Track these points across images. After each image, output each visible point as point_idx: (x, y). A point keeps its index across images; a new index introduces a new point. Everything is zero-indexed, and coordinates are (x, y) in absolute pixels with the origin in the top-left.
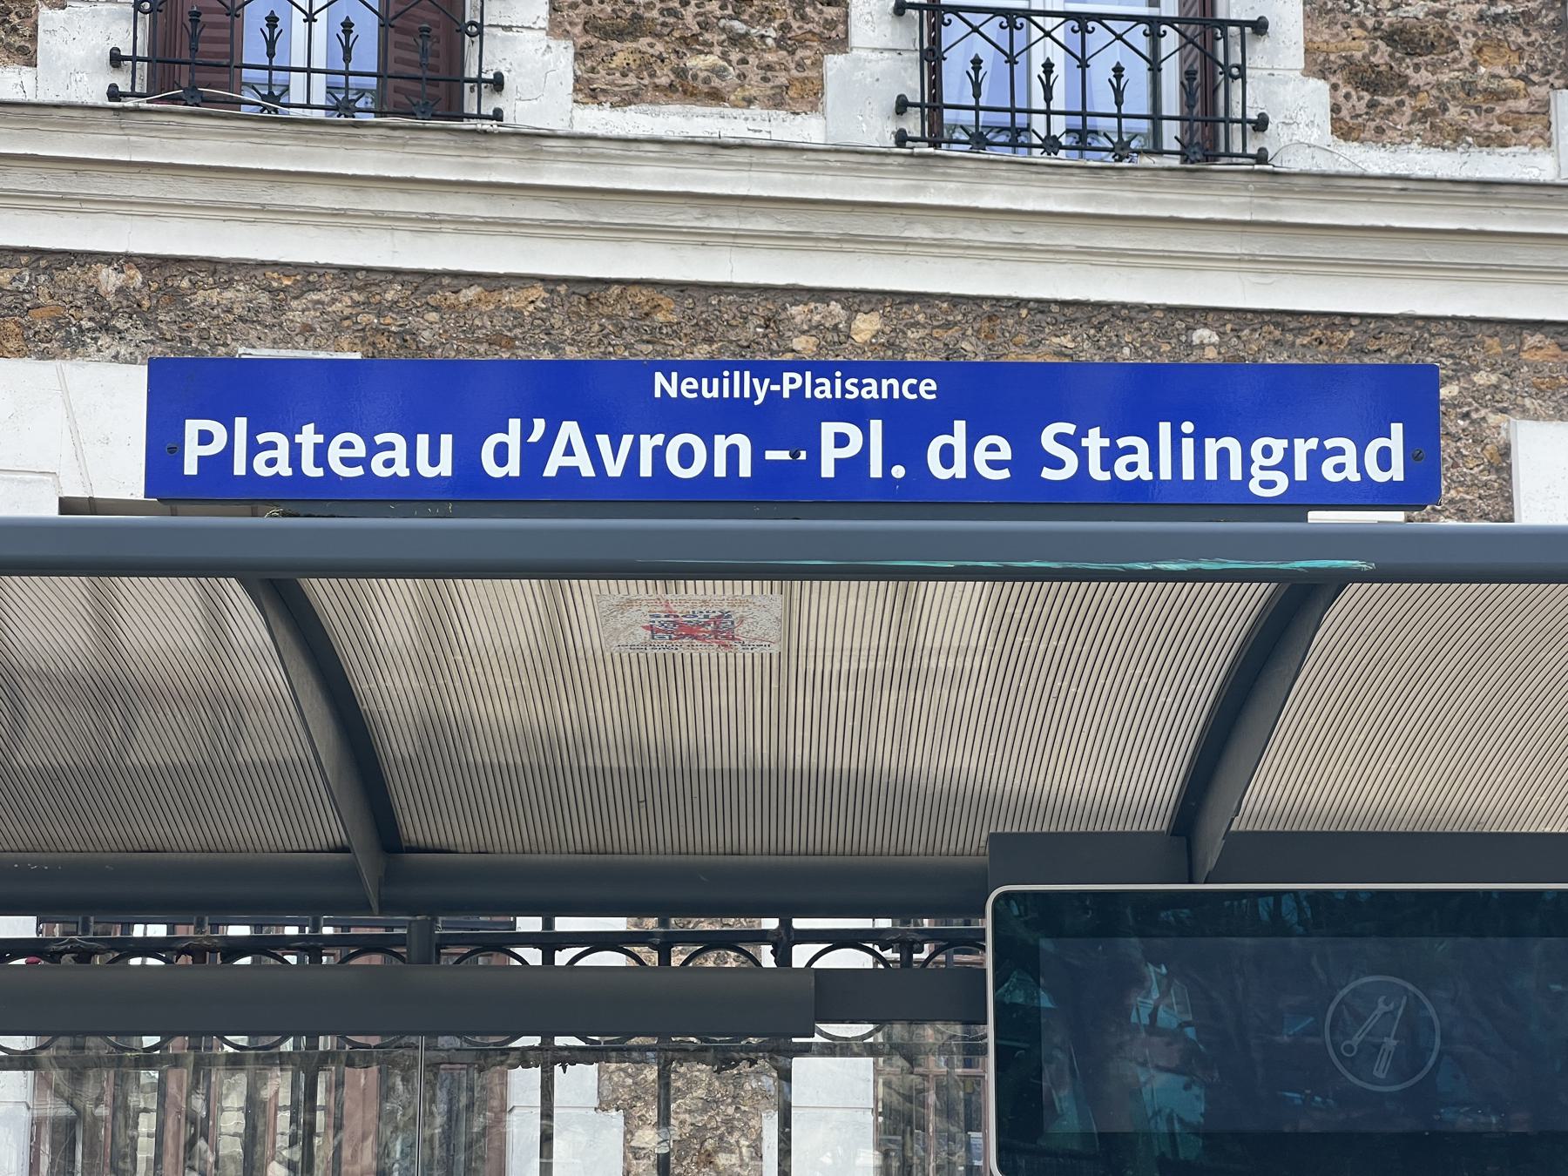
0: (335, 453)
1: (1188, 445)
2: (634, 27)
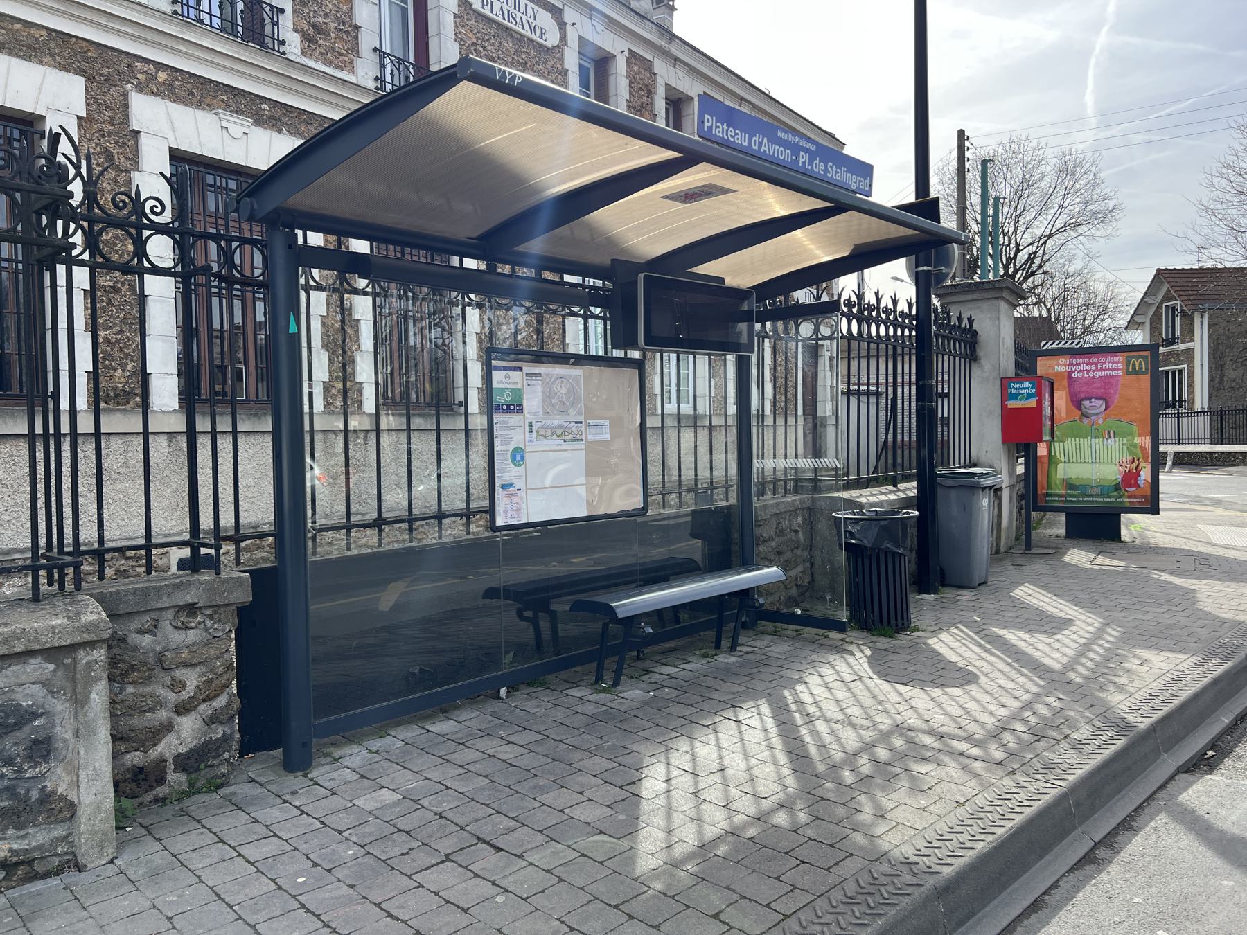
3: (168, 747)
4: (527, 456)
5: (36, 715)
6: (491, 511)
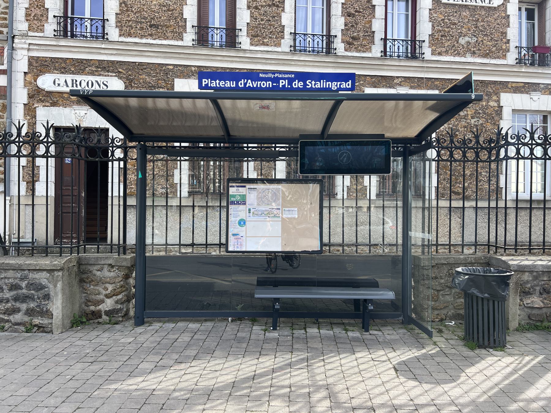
0: (221, 84)
1: (325, 83)
2: (257, 36)
3: (103, 307)
4: (247, 223)
6: (227, 245)
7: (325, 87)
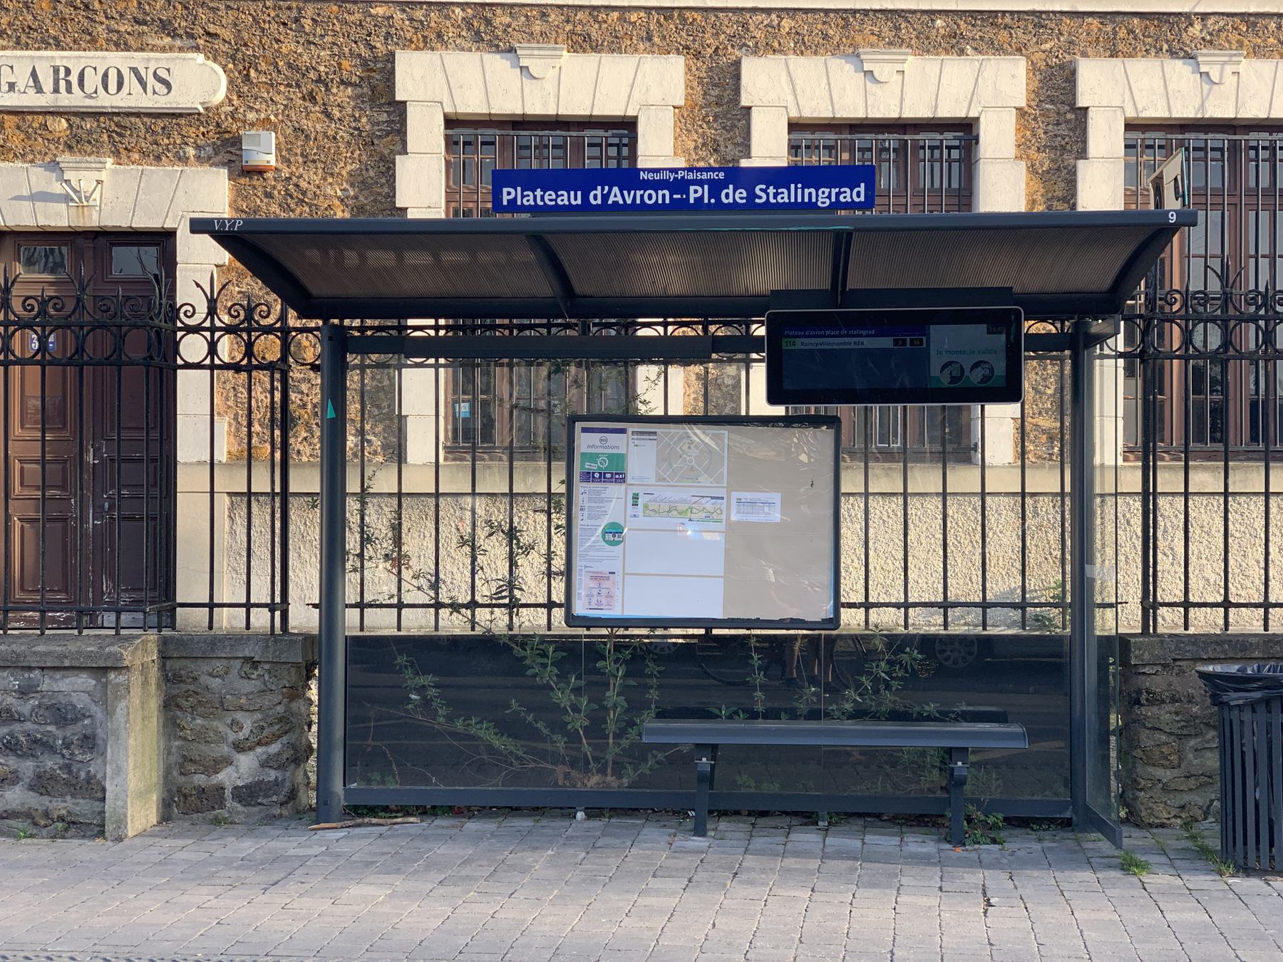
0: (546, 198)
1: (799, 191)
3: (227, 778)
5: (85, 716)
6: (568, 605)
7: (799, 200)
